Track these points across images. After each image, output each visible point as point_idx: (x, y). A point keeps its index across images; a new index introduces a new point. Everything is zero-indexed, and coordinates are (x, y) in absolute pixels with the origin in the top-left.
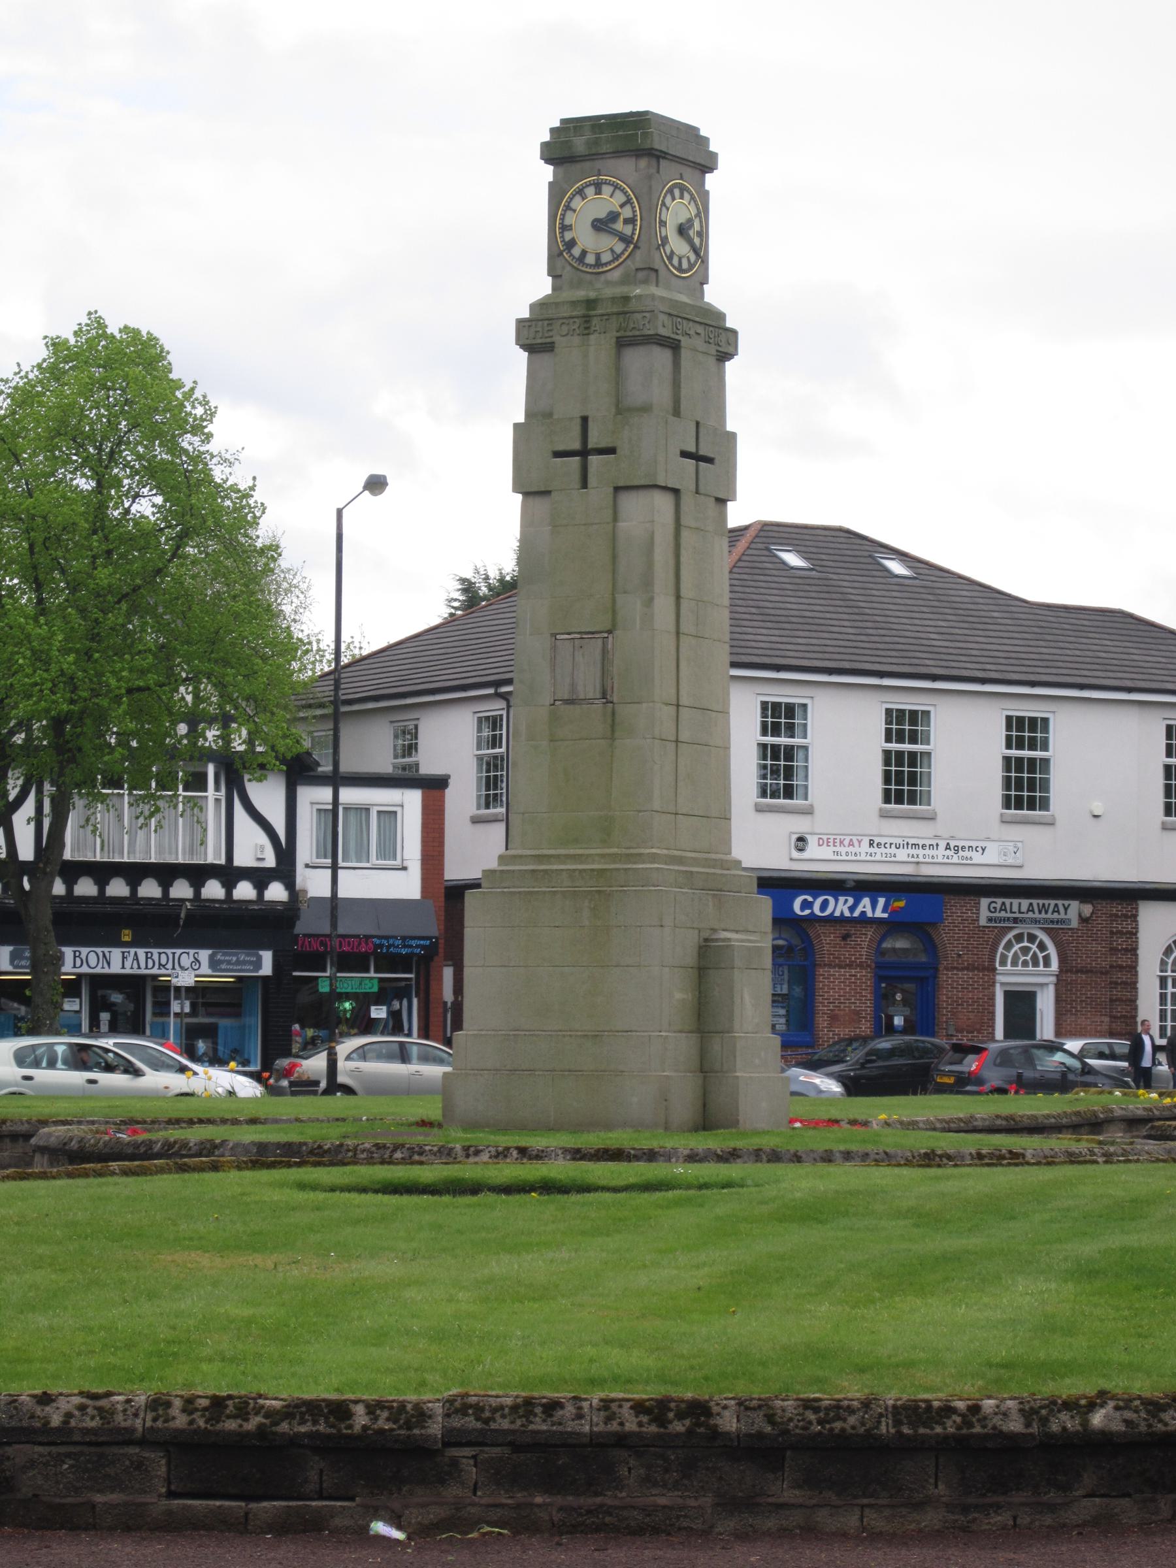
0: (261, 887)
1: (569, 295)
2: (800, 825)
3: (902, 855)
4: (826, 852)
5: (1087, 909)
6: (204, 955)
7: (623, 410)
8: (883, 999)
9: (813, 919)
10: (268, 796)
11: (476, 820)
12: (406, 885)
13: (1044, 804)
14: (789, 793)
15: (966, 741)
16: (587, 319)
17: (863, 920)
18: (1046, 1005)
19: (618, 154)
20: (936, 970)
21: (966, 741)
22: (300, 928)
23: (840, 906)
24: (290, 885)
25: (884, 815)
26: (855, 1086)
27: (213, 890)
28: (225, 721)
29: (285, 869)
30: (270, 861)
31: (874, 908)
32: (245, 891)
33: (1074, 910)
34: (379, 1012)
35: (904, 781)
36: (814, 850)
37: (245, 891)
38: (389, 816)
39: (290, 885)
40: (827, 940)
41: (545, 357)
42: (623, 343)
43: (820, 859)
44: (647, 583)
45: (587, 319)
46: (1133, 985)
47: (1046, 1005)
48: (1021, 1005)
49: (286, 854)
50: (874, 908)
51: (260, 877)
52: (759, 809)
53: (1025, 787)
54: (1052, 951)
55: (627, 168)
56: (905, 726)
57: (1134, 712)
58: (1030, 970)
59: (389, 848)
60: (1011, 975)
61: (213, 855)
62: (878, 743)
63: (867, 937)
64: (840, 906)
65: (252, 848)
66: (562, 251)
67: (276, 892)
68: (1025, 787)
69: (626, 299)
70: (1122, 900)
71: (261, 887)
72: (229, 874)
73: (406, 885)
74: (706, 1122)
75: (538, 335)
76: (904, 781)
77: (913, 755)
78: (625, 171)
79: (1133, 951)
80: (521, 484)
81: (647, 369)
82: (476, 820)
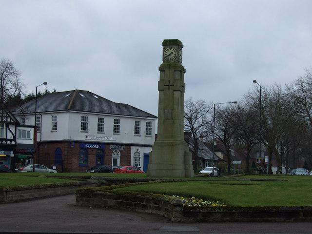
0: (11, 142)
1: (166, 64)
2: (86, 134)
3: (100, 139)
4: (90, 138)
5: (124, 147)
6: (3, 152)
7: (175, 80)
8: (97, 160)
9: (88, 148)
10: (12, 128)
11: (51, 132)
12: (31, 142)
13: (151, 134)
14: (85, 129)
15: (109, 123)
16: (169, 67)
17: (95, 148)
18: (119, 160)
19: (173, 45)
20: (104, 155)
21: (109, 123)
22: (17, 148)
23: (92, 146)
24: (15, 142)
25: (98, 133)
26: (58, 172)
27: (4, 142)
28: (7, 117)
29: (15, 139)
30: (13, 138)
31: (96, 146)
32: (9, 142)
33: (123, 147)
34: (27, 161)
35: (100, 128)
36: (88, 138)
37: (9, 142)
38: (29, 132)
39: (15, 142)
40: (90, 151)
41: (163, 72)
42: (175, 71)
43: (89, 139)
44: (178, 104)
45: (169, 67)
46: (130, 158)
47: (119, 160)
48: (115, 160)
49: (15, 137)
50: (96, 146)
51: (11, 140)
52: (81, 132)
53: (116, 129)
54: (120, 153)
55: (175, 47)
56: (101, 120)
57: (131, 119)
58: (117, 156)
59: (29, 137)
60: (114, 156)
61: (4, 137)
62: (97, 123)
63: (95, 151)
64: (92, 146)
65: (10, 136)
66: (165, 58)
67: (13, 143)
68: (116, 129)
69: (176, 64)
70: (129, 146)
71: (11, 142)
72: (6, 140)
73: (31, 142)
74: (186, 176)
75: (161, 69)
76: (100, 128)
77: (102, 124)
78: (172, 46)
79: (130, 153)
80: (159, 89)
81: (177, 74)
82: (51, 132)
